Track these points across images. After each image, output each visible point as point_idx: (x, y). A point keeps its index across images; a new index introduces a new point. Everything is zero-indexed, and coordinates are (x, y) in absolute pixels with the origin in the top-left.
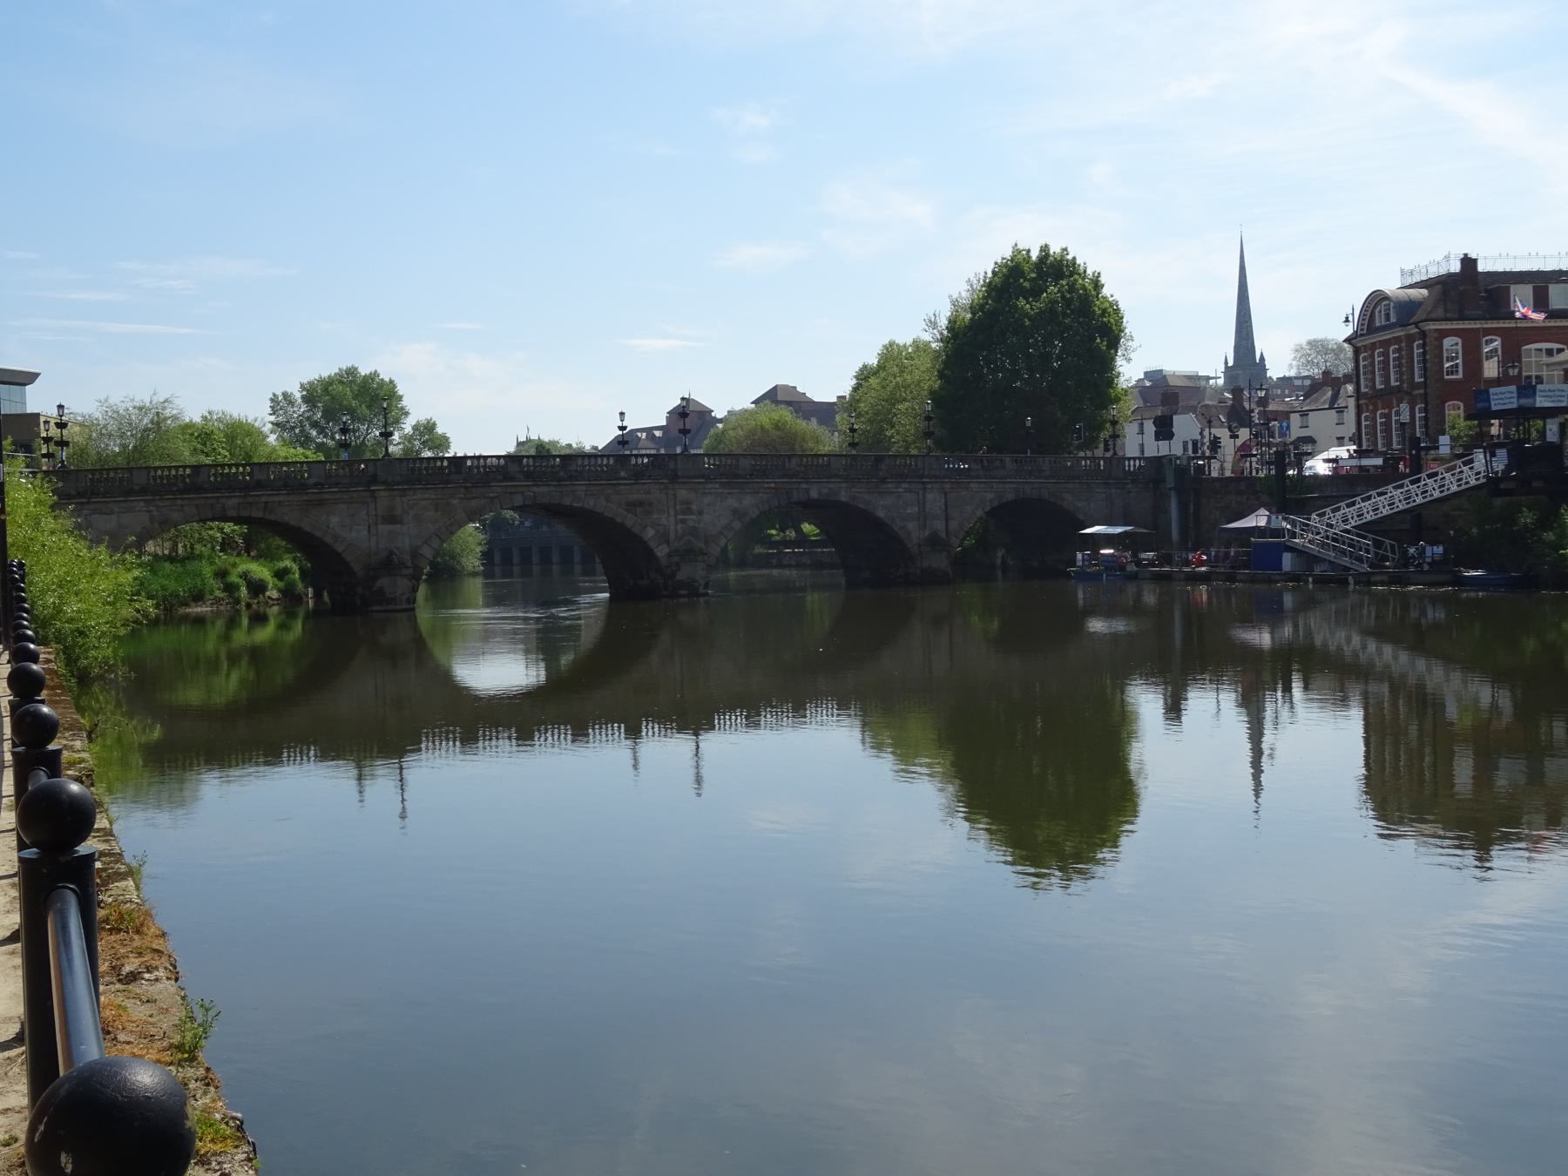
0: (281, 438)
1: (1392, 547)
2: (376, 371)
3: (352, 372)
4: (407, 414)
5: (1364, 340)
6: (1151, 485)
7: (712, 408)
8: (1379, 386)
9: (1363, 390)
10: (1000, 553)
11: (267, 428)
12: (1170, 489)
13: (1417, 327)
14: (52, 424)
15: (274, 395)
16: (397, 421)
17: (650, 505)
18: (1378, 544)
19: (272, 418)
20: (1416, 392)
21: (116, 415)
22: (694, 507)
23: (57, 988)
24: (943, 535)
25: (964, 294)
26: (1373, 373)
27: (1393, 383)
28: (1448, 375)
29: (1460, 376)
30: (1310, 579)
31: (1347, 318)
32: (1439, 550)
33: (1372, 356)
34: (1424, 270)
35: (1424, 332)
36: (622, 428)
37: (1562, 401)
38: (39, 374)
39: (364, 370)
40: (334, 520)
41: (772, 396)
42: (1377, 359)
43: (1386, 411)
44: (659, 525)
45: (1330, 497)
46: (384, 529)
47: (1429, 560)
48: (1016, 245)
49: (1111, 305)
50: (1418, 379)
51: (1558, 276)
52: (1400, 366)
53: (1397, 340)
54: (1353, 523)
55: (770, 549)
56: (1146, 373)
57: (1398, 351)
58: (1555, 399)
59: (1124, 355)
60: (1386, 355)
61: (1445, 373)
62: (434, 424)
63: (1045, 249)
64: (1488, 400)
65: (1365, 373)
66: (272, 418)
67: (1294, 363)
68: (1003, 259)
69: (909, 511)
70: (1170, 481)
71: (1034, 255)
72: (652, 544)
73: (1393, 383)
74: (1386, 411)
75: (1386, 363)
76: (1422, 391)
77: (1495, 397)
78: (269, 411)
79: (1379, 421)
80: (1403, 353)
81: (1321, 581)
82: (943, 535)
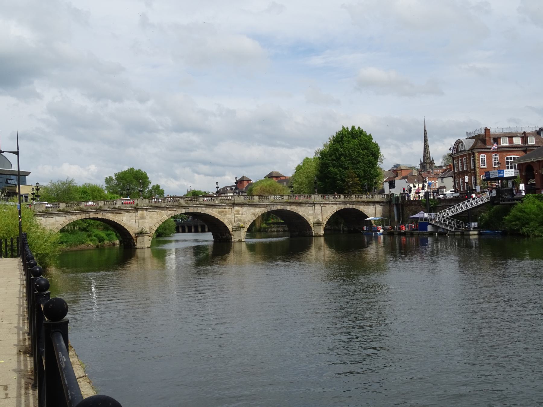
0: (109, 192)
1: (462, 223)
2: (140, 169)
3: (132, 169)
4: (150, 183)
5: (455, 156)
6: (388, 203)
7: (250, 179)
8: (460, 170)
9: (456, 171)
10: (342, 225)
11: (104, 188)
12: (394, 204)
13: (471, 151)
14: (35, 189)
15: (106, 178)
16: (147, 185)
17: (226, 212)
18: (458, 222)
19: (106, 185)
20: (472, 172)
21: (54, 185)
22: (240, 212)
23: (38, 380)
24: (321, 220)
25: (328, 143)
26: (458, 165)
27: (465, 169)
28: (485, 165)
29: (486, 167)
30: (436, 234)
31: (450, 148)
32: (476, 223)
33: (458, 160)
34: (474, 133)
35: (474, 152)
36: (217, 187)
37: (496, 176)
38: (30, 173)
39: (136, 169)
40: (125, 218)
41: (270, 176)
42: (459, 161)
43: (463, 178)
44: (229, 218)
45: (444, 206)
46: (141, 221)
47: (473, 227)
48: (343, 127)
49: (375, 145)
50: (472, 168)
51: (542, 130)
52: (467, 163)
53: (466, 155)
54: (450, 215)
55: (268, 225)
56: (394, 165)
57: (466, 159)
58: (510, 174)
59: (380, 161)
60: (462, 160)
61: (484, 167)
62: (159, 186)
63: (353, 127)
64: (503, 173)
65: (456, 166)
66: (106, 185)
67: (443, 161)
68: (339, 131)
69: (310, 213)
70: (394, 202)
71: (350, 129)
72: (226, 224)
73: (465, 169)
74: (463, 178)
75: (462, 163)
76: (474, 171)
77: (491, 174)
78: (105, 183)
79: (461, 181)
80: (468, 159)
81: (440, 234)
82: (321, 220)
